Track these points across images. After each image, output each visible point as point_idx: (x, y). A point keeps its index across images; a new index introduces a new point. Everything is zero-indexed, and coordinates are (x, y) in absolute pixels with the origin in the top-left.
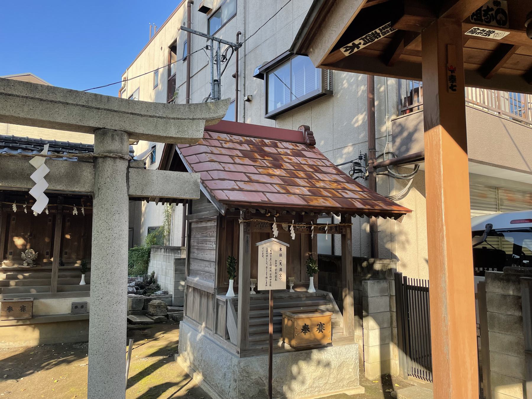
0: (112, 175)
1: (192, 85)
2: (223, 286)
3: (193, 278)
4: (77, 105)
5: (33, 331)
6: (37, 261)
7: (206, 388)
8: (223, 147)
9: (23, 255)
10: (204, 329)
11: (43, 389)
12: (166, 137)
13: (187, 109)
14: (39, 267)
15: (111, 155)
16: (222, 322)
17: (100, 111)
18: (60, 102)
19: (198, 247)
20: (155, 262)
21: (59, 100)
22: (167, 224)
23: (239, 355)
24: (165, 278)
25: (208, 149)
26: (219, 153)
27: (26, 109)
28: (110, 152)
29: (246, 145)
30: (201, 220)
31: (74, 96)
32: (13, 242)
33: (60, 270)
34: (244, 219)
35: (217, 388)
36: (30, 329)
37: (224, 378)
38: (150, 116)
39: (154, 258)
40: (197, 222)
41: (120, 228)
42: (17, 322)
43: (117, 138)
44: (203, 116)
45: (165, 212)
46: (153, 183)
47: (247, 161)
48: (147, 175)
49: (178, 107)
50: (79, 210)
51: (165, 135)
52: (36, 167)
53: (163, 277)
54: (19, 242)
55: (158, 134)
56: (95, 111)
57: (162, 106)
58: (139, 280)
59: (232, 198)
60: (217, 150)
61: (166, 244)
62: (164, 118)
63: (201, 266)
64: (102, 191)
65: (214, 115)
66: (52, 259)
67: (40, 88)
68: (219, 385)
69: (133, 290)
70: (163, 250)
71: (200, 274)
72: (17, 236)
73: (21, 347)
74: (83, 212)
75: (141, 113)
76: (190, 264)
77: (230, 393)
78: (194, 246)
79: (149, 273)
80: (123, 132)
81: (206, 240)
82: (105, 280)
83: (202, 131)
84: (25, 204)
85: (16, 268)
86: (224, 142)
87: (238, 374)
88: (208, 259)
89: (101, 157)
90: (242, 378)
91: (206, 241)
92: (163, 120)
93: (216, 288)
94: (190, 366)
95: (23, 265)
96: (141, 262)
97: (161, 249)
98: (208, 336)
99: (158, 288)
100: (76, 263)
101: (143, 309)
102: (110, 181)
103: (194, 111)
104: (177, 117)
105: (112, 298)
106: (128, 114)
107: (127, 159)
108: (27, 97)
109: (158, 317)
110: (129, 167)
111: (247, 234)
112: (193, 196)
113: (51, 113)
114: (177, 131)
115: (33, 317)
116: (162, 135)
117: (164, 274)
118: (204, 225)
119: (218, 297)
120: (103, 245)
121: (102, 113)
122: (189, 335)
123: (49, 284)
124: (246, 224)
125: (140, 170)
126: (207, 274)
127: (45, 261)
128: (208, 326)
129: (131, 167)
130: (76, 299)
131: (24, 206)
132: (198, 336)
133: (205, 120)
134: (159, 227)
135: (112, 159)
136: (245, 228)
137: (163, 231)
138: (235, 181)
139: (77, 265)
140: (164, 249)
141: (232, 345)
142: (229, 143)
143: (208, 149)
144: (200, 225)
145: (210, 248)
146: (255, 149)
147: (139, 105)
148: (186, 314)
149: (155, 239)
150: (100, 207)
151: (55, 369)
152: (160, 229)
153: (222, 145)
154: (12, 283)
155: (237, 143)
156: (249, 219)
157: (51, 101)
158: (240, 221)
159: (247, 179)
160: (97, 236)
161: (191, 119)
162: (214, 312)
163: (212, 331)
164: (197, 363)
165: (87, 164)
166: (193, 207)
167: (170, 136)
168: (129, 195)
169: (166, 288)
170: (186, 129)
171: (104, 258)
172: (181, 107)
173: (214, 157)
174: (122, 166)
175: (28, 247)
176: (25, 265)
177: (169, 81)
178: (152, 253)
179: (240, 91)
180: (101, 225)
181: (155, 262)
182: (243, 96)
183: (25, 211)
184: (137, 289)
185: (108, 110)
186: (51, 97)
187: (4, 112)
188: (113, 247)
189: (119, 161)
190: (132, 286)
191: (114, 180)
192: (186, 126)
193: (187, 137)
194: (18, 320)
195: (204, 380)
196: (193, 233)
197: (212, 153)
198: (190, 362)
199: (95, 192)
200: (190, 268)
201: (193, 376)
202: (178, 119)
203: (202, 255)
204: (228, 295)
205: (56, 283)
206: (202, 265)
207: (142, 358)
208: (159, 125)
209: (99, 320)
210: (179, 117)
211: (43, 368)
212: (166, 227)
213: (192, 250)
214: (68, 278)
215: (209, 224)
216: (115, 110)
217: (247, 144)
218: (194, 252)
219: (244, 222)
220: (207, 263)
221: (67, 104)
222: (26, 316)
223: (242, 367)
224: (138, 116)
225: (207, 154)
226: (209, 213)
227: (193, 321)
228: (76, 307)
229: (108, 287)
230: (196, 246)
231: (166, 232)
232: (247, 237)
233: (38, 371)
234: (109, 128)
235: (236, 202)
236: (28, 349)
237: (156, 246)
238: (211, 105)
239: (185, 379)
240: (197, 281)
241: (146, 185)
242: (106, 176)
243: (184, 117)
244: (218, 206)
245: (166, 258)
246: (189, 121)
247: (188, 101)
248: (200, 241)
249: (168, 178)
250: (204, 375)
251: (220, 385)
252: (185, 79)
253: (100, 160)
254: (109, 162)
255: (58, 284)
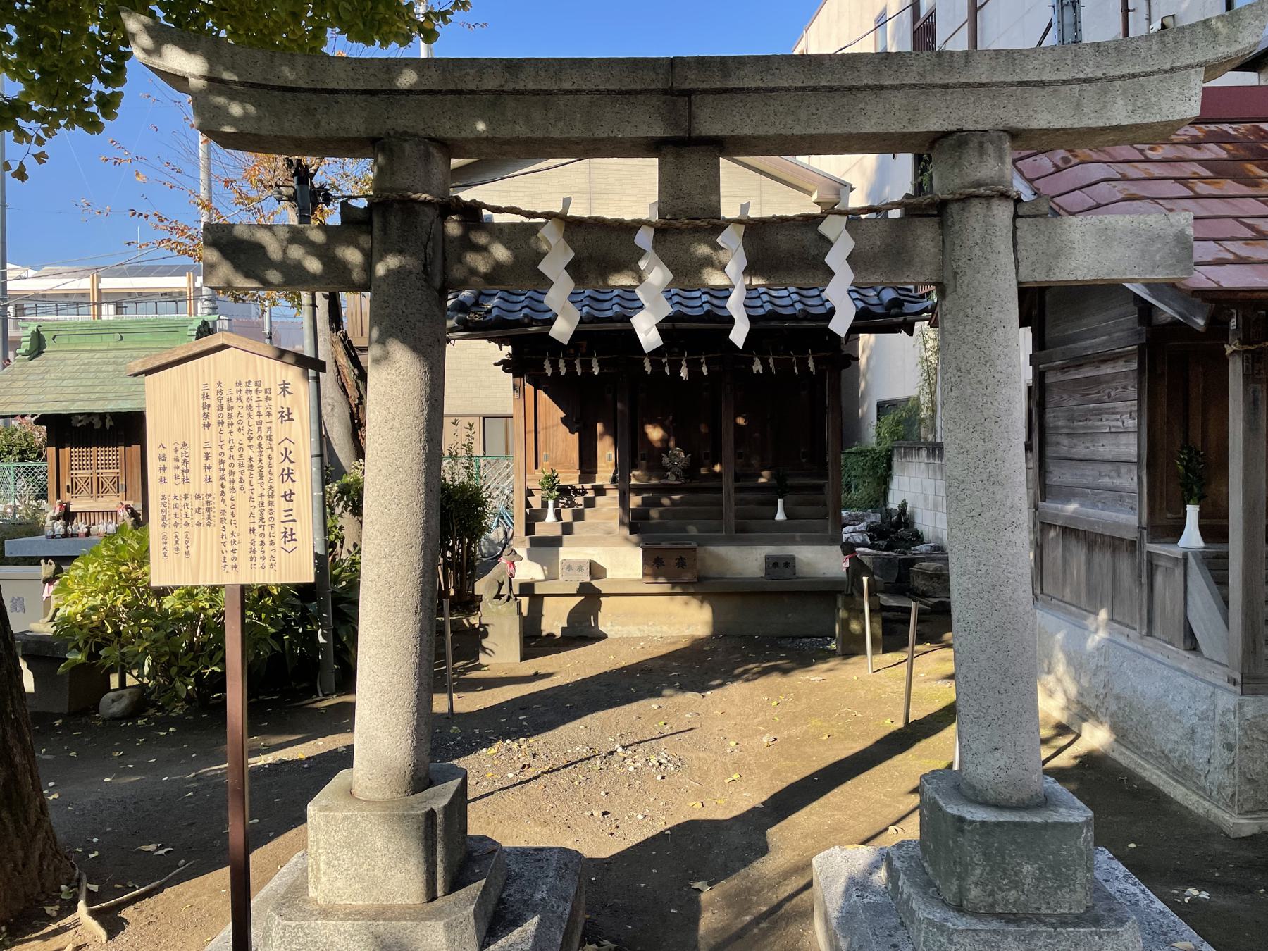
0: (983, 239)
1: (982, 29)
2: (1164, 523)
3: (1060, 506)
4: (902, 86)
5: (701, 607)
6: (690, 471)
7: (1126, 758)
8: (1148, 161)
9: (665, 459)
10: (1107, 625)
11: (757, 716)
12: (1103, 129)
13: (1155, 47)
14: (695, 484)
15: (982, 191)
16: (1169, 608)
17: (950, 90)
18: (868, 87)
19: (1073, 429)
20: (906, 479)
21: (865, 82)
22: (927, 390)
23: (1238, 689)
24: (935, 515)
25: (1113, 171)
26: (1143, 175)
27: (803, 115)
28: (978, 184)
29: (1211, 146)
30: (1079, 362)
31: (895, 67)
32: (645, 434)
33: (738, 490)
34: (1242, 343)
35: (1164, 762)
36: (694, 603)
37: (1192, 739)
38: (1065, 83)
39: (902, 470)
40: (1064, 369)
41: (1007, 359)
42: (673, 588)
43: (990, 149)
44: (1199, 58)
45: (922, 363)
46: (1074, 248)
47: (1230, 187)
48: (1059, 231)
49: (1132, 46)
50: (764, 363)
51: (1102, 125)
52: (832, 238)
53: (929, 514)
54: (655, 433)
55: (1085, 123)
56: (939, 93)
57: (1091, 51)
58: (873, 519)
59: (1226, 284)
60: (1136, 170)
61: (925, 438)
62: (1098, 80)
63: (1083, 476)
64: (964, 278)
65: (1228, 50)
66: (717, 468)
67: (827, 62)
68: (1171, 755)
69: (864, 540)
70: (924, 452)
71: (1085, 495)
72: (650, 423)
73: (684, 637)
74: (772, 365)
75: (1044, 79)
76: (1046, 472)
77: (1209, 775)
78: (1057, 428)
79: (894, 503)
80: (1002, 133)
81: (1100, 409)
82: (985, 476)
83: (1195, 98)
84: (664, 357)
85: (654, 485)
86: (1147, 146)
87: (1239, 733)
88: (1109, 457)
89: (958, 200)
90: (1248, 744)
91: (1098, 413)
92: (1095, 86)
93: (1144, 525)
94: (1067, 708)
95: (666, 478)
96: (870, 479)
97: (919, 449)
98: (1123, 640)
99: (918, 538)
100: (761, 476)
101: (899, 580)
102: (981, 254)
103: (1175, 48)
104: (1131, 72)
105: (1002, 514)
106: (1012, 85)
107: (1012, 198)
108: (803, 89)
109: (935, 600)
110: (1016, 216)
111: (1254, 382)
112: (1175, 274)
113: (851, 115)
114: (1130, 108)
115: (701, 579)
116: (1094, 126)
117: (930, 506)
118: (1089, 372)
119: (1157, 548)
120: (973, 398)
121: (955, 95)
122: (1059, 637)
123: (720, 516)
124: (1249, 356)
125: (1041, 220)
126: (1107, 494)
127: (703, 471)
128: (1116, 617)
129: (1022, 217)
130: (773, 548)
131: (664, 360)
132: (1090, 640)
133: (1203, 69)
134: (908, 400)
135: (983, 201)
136: (1247, 367)
137: (919, 408)
138: (1215, 240)
139: (762, 480)
140: (928, 450)
141: (1209, 663)
142: (1163, 148)
143: (1113, 171)
144: (1073, 375)
145: (1113, 430)
146: (1243, 153)
147: (1036, 59)
148: (1042, 590)
149: (901, 428)
150: (961, 315)
151: (761, 681)
152: (910, 403)
153: (1145, 156)
154: (654, 513)
155: (1184, 143)
156: (1259, 343)
157: (851, 89)
158: (1229, 349)
159: (1249, 233)
160: (959, 379)
161: (1166, 72)
162: (1141, 584)
163: (1135, 629)
164: (1089, 702)
165: (925, 219)
166: (1047, 331)
167: (1114, 124)
168: (1019, 283)
169: (937, 538)
170: (1154, 99)
171: (977, 428)
172: (1139, 43)
173: (1133, 189)
174: (1003, 212)
175: (672, 444)
176: (672, 480)
177: (915, 32)
178: (895, 459)
179: (1133, 10)
180: (967, 355)
181: (906, 479)
182: (1146, 22)
183: (667, 370)
184: (871, 538)
185: (968, 85)
186: (849, 80)
187: (766, 128)
188: (996, 404)
189: (998, 202)
190: (862, 532)
191: (989, 249)
192: (1155, 90)
193: (1158, 119)
194: (674, 585)
195: (1116, 740)
196: (1053, 398)
197: (1125, 178)
198: (1068, 699)
199: (945, 282)
200: (1047, 482)
201: (1080, 729)
202: (1134, 76)
203: (1088, 448)
204: (1182, 543)
205: (732, 515)
206: (1087, 472)
207: (937, 680)
208: (1085, 101)
209: (976, 560)
210: (1137, 70)
211: (737, 678)
212: (924, 399)
213: (1051, 438)
214: (752, 506)
215: (1120, 367)
216: (984, 80)
217: (1216, 143)
218: (1058, 443)
219: (1245, 352)
220: (1106, 468)
221: (882, 87)
222: (688, 577)
223: (1249, 717)
224: (1035, 88)
225: (1114, 183)
226: (1106, 340)
227: (1068, 606)
228: (775, 565)
229: (991, 490)
230: (1063, 427)
231: (925, 409)
232: (1254, 392)
233: (732, 682)
234: (972, 128)
235: (1241, 294)
236: (696, 640)
237: (905, 443)
238: (1220, 25)
239: (1058, 735)
240: (1074, 512)
241: (1057, 256)
242: (971, 243)
243: (1149, 69)
244: (1183, 311)
245: (934, 468)
246: (1161, 76)
247: (1126, 34)
248: (1076, 414)
249: (1109, 232)
250: (1114, 728)
251: (1177, 755)
252: (964, 14)
253: (954, 208)
254: (977, 208)
255: (736, 517)
